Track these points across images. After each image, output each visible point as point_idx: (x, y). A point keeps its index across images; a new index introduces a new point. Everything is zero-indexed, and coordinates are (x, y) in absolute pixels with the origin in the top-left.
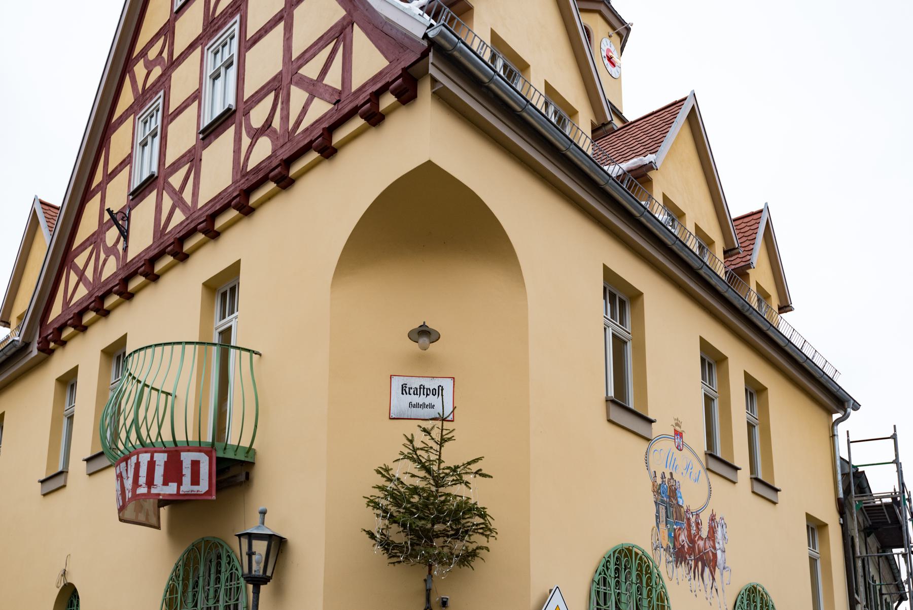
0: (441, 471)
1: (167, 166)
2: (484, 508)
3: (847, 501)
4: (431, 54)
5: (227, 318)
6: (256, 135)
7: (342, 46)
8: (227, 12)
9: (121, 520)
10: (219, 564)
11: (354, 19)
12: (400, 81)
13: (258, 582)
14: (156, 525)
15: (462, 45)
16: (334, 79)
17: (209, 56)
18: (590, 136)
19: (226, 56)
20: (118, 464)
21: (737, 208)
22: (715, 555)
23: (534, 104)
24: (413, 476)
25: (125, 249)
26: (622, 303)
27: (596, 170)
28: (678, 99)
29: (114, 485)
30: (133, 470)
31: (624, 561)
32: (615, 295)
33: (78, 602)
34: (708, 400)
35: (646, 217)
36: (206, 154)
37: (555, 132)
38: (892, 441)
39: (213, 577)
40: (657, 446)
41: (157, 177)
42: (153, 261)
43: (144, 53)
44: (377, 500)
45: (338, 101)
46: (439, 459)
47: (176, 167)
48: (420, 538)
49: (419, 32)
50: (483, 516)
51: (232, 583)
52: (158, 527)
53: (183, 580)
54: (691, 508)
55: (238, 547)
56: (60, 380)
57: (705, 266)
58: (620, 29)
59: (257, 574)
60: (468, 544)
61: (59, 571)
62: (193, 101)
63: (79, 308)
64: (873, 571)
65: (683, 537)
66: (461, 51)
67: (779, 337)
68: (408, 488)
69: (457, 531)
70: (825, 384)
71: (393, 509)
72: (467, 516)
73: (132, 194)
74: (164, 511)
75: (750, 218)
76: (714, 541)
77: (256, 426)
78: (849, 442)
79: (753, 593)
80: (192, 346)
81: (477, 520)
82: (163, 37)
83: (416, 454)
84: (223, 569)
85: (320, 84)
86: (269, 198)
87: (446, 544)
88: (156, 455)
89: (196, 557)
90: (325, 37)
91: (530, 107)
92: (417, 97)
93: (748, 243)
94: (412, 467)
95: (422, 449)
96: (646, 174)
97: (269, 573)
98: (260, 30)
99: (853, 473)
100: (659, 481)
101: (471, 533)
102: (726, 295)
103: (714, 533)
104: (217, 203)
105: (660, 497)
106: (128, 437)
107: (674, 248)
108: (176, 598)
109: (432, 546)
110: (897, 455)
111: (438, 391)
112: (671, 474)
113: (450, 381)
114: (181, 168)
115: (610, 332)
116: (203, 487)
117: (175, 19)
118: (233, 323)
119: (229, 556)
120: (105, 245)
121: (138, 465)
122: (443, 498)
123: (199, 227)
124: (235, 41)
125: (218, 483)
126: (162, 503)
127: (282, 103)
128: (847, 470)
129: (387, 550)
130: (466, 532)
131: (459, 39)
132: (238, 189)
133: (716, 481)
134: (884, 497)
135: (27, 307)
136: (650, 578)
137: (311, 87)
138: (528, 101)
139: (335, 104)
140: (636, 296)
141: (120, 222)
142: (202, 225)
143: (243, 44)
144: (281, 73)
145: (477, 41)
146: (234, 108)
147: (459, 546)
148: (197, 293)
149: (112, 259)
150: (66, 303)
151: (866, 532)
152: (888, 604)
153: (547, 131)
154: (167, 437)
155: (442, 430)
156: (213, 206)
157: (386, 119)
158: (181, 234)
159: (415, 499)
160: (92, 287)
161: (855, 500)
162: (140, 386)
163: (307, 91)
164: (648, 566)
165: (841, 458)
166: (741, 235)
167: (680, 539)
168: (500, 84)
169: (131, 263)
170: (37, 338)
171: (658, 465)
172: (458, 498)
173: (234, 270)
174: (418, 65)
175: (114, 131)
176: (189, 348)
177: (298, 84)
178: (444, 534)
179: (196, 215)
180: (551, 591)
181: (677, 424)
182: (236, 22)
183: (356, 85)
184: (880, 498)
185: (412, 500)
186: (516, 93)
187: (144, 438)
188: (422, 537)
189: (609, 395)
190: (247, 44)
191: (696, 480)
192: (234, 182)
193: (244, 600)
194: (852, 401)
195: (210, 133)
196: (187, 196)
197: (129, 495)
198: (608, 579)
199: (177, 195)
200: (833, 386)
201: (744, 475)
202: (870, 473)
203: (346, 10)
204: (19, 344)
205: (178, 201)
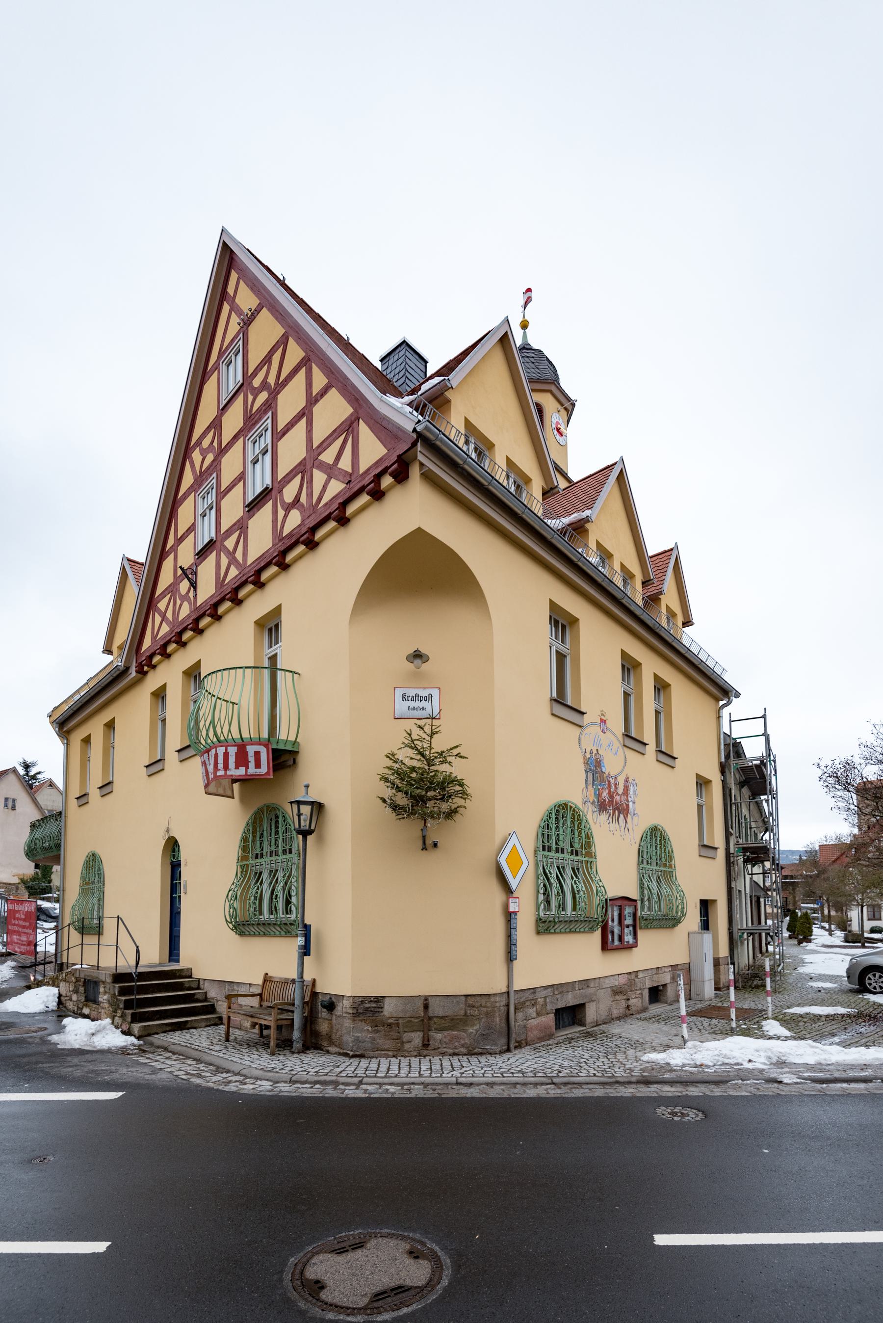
0: (432, 755)
1: (222, 532)
2: (462, 780)
3: (727, 764)
4: (419, 444)
5: (274, 648)
6: (288, 508)
7: (351, 437)
8: (261, 409)
9: (206, 793)
10: (277, 822)
11: (360, 415)
12: (396, 465)
13: (306, 834)
14: (231, 796)
15: (442, 435)
16: (345, 464)
17: (250, 445)
18: (541, 500)
19: (263, 446)
20: (202, 755)
21: (652, 549)
22: (628, 806)
23: (497, 479)
24: (412, 759)
25: (195, 596)
26: (564, 627)
27: (544, 527)
28: (610, 463)
29: (200, 770)
30: (213, 759)
31: (561, 812)
32: (558, 621)
33: (179, 849)
34: (626, 695)
35: (582, 562)
36: (252, 523)
37: (514, 500)
38: (762, 720)
39: (273, 830)
40: (587, 731)
41: (215, 541)
42: (216, 606)
43: (199, 443)
44: (387, 776)
45: (349, 482)
46: (430, 747)
47: (229, 533)
48: (418, 802)
49: (409, 427)
50: (461, 785)
51: (287, 834)
52: (233, 797)
53: (253, 833)
54: (611, 774)
55: (290, 811)
56: (153, 694)
57: (626, 597)
58: (567, 405)
59: (304, 828)
60: (451, 804)
61: (165, 828)
62: (239, 481)
63: (164, 641)
64: (745, 811)
65: (605, 794)
66: (442, 441)
67: (682, 648)
68: (408, 768)
69: (444, 795)
70: (714, 679)
71: (398, 782)
72: (450, 785)
73: (197, 554)
74: (236, 786)
75: (663, 555)
76: (627, 796)
77: (299, 726)
78: (731, 721)
79: (655, 830)
80: (250, 670)
81: (458, 788)
82: (213, 430)
83: (414, 743)
84: (280, 825)
85: (335, 467)
86: (300, 557)
87: (436, 805)
88: (228, 748)
89: (261, 817)
90: (338, 430)
91: (494, 481)
92: (408, 477)
93: (661, 575)
94: (411, 752)
95: (418, 740)
96: (584, 526)
97: (313, 827)
98: (287, 424)
99: (733, 744)
100: (588, 755)
101: (453, 797)
102: (642, 617)
103: (627, 790)
104: (261, 561)
105: (588, 767)
106: (207, 734)
107: (604, 584)
108: (249, 845)
109: (426, 807)
110: (765, 730)
111: (429, 698)
112: (597, 750)
113: (437, 691)
114: (233, 534)
115: (554, 649)
116: (264, 769)
117: (222, 415)
118: (278, 651)
119: (284, 816)
120: (180, 593)
121: (216, 755)
122: (433, 774)
123: (249, 579)
124: (269, 433)
125: (274, 766)
126: (234, 781)
127: (307, 483)
128: (728, 742)
129: (395, 810)
130: (450, 796)
131: (440, 431)
132: (277, 550)
133: (630, 754)
134: (754, 760)
135: (126, 638)
136: (580, 823)
137: (329, 470)
138: (493, 477)
139: (347, 484)
140: (574, 621)
141: (190, 576)
142: (251, 578)
143: (275, 436)
144: (305, 459)
145: (454, 431)
146: (270, 487)
147: (445, 806)
148: (249, 629)
149: (186, 604)
150: (154, 637)
151: (741, 784)
152: (756, 835)
153: (507, 499)
154: (236, 735)
155: (432, 726)
156: (259, 563)
157: (386, 495)
158: (236, 585)
159: (414, 775)
160: (172, 625)
161: (733, 762)
162: (214, 699)
163: (325, 473)
164: (579, 815)
165: (724, 733)
166: (656, 569)
167: (603, 796)
168: (471, 468)
169: (200, 607)
170: (134, 664)
171: (588, 745)
172: (444, 773)
173: (277, 611)
174: (410, 452)
175: (180, 505)
176: (248, 671)
177: (318, 468)
178: (434, 798)
179: (246, 570)
180: (510, 834)
181: (602, 715)
182: (269, 417)
183: (362, 469)
184: (752, 761)
185: (411, 775)
186: (484, 472)
187: (219, 734)
188: (419, 800)
189: (553, 696)
190: (278, 435)
191: (616, 754)
192: (274, 545)
193: (296, 845)
194: (735, 691)
195: (253, 506)
196: (239, 555)
197: (211, 776)
198: (550, 825)
199: (231, 555)
200: (720, 681)
201: (651, 749)
202: (745, 743)
203: (353, 408)
204: (122, 668)
205: (233, 560)
